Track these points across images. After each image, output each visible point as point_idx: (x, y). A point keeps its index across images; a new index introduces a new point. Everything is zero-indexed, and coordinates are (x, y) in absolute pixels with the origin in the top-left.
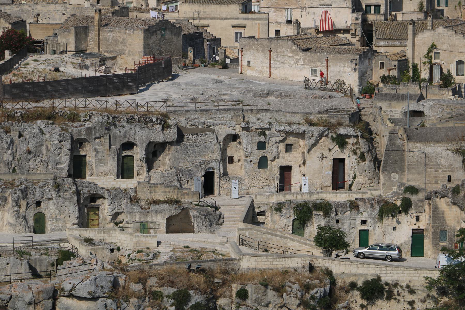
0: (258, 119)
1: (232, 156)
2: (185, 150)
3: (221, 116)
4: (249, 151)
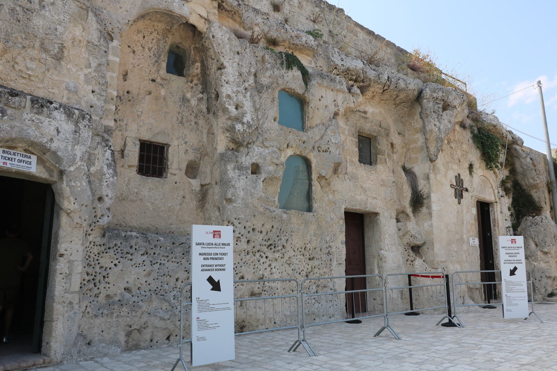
1: (160, 139)
4: (248, 118)
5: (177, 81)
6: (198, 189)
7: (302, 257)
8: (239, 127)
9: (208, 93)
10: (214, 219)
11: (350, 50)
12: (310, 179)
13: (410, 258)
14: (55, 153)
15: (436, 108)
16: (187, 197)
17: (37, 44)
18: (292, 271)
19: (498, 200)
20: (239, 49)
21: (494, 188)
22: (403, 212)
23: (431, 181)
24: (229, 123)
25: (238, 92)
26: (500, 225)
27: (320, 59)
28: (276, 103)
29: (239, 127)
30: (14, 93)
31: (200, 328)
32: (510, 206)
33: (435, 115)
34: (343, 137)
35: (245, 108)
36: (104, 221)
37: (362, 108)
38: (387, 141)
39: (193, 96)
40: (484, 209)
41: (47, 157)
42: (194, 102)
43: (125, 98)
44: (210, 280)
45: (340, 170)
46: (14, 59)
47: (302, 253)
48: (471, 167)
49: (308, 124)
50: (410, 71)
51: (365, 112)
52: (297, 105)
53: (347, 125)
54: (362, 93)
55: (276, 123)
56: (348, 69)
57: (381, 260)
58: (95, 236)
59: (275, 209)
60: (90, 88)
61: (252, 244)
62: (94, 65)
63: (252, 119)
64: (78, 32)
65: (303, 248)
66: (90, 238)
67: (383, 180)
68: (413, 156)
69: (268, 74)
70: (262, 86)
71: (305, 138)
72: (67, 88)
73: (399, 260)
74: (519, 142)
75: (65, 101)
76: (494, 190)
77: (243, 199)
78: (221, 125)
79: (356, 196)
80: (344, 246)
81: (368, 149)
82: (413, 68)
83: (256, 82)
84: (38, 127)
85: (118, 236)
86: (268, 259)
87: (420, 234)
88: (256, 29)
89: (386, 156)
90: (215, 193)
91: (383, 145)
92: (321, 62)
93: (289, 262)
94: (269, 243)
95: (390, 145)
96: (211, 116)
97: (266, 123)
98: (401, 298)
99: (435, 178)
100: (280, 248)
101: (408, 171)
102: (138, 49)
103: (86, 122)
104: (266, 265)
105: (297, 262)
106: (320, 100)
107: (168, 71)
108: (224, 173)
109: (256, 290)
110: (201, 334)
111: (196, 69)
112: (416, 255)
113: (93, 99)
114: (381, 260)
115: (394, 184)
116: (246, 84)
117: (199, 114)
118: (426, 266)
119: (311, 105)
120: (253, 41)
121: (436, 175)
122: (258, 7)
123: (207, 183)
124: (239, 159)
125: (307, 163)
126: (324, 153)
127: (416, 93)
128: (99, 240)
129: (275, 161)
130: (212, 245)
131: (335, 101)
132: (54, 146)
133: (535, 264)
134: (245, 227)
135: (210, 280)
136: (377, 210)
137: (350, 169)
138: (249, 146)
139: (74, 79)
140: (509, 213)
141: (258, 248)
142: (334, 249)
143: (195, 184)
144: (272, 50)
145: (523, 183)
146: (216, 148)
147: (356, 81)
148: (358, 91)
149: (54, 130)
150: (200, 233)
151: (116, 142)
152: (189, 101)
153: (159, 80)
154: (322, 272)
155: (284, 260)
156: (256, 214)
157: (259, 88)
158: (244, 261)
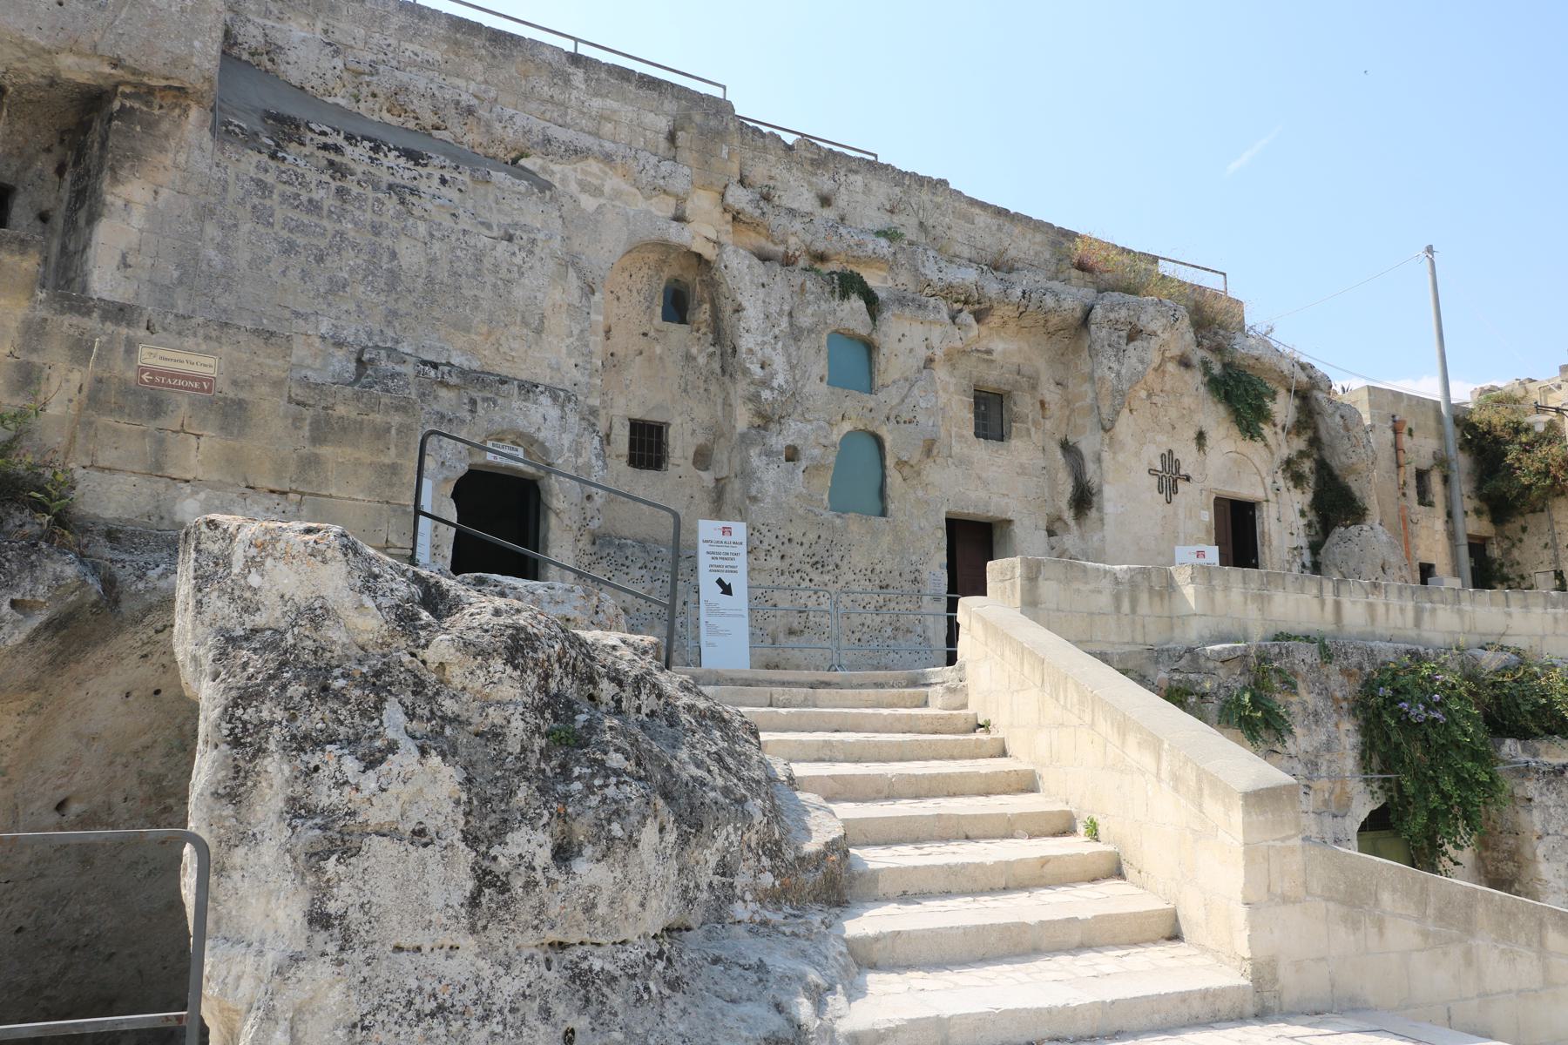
0: (825, 201)
1: (655, 417)
2: (300, 228)
3: (596, 103)
4: (779, 380)
5: (677, 331)
6: (712, 485)
8: (766, 394)
9: (722, 346)
11: (957, 249)
12: (883, 467)
14: (542, 444)
15: (1114, 337)
16: (697, 496)
17: (519, 319)
19: (1271, 497)
20: (764, 280)
22: (1060, 519)
23: (1104, 465)
24: (752, 389)
25: (764, 343)
26: (1275, 543)
27: (903, 271)
28: (824, 354)
29: (766, 394)
30: (503, 381)
31: (709, 633)
32: (1306, 508)
33: (1110, 352)
34: (943, 398)
36: (594, 524)
37: (983, 345)
38: (1033, 397)
39: (700, 352)
41: (534, 448)
42: (702, 360)
43: (612, 362)
44: (720, 582)
45: (935, 451)
46: (498, 340)
48: (1201, 437)
49: (878, 381)
50: (1075, 273)
51: (989, 352)
52: (863, 351)
53: (952, 375)
54: (978, 321)
55: (824, 384)
56: (950, 286)
58: (584, 543)
60: (573, 361)
62: (576, 332)
64: (557, 295)
66: (580, 545)
67: (1022, 466)
68: (1079, 422)
69: (809, 311)
70: (801, 330)
71: (872, 404)
72: (550, 366)
74: (1322, 386)
75: (547, 381)
76: (1263, 479)
77: (773, 497)
78: (740, 392)
81: (992, 414)
82: (1082, 267)
83: (791, 325)
84: (526, 416)
85: (611, 543)
88: (792, 240)
90: (734, 490)
91: (1024, 405)
92: (904, 278)
95: (1038, 405)
96: (726, 379)
101: (1067, 448)
102: (624, 294)
103: (572, 405)
107: (665, 318)
108: (746, 461)
109: (795, 626)
110: (712, 639)
111: (703, 314)
113: (577, 375)
116: (777, 331)
119: (884, 350)
120: (788, 261)
122: (795, 206)
125: (879, 441)
127: (1078, 314)
128: (589, 549)
129: (823, 441)
130: (719, 544)
132: (541, 436)
135: (720, 582)
136: (1009, 515)
137: (957, 448)
139: (554, 356)
140: (1303, 521)
141: (797, 566)
142: (925, 575)
143: (708, 478)
144: (817, 271)
145: (1333, 464)
147: (966, 302)
148: (971, 320)
149: (540, 417)
150: (708, 529)
151: (602, 426)
152: (695, 359)
153: (652, 333)
154: (902, 607)
157: (796, 334)
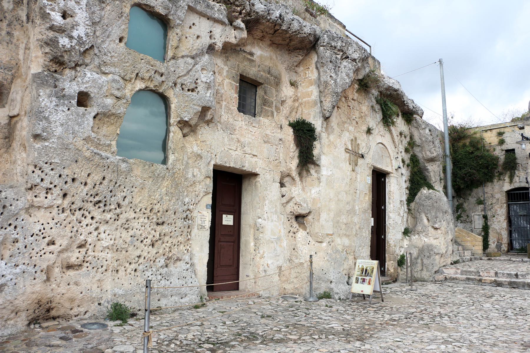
4: (80, 31)
7: (146, 220)
8: (64, 41)
10: (19, 162)
12: (168, 124)
13: (292, 230)
15: (334, 58)
18: (130, 239)
21: (392, 159)
22: (289, 175)
24: (51, 34)
35: (76, 19)
40: (379, 178)
47: (146, 216)
51: (252, 54)
53: (226, 64)
57: (258, 230)
59: (109, 155)
61: (68, 199)
63: (87, 35)
65: (149, 210)
73: (280, 231)
74: (419, 112)
77: (59, 138)
79: (230, 151)
80: (210, 211)
86: (94, 221)
87: (305, 201)
89: (274, 108)
93: (126, 226)
94: (97, 199)
97: (107, 42)
98: (279, 276)
99: (328, 138)
100: (113, 207)
104: (91, 228)
105: (139, 227)
106: (190, 27)
112: (300, 226)
114: (258, 230)
115: (281, 142)
117: (15, 22)
118: (310, 239)
121: (328, 134)
123: (16, 114)
124: (60, 85)
126: (190, 93)
131: (211, 32)
133: (426, 240)
134: (60, 176)
137: (225, 117)
138: (78, 69)
141: (78, 204)
146: (29, 67)
155: (119, 223)
156: (80, 159)
158: (56, 221)
